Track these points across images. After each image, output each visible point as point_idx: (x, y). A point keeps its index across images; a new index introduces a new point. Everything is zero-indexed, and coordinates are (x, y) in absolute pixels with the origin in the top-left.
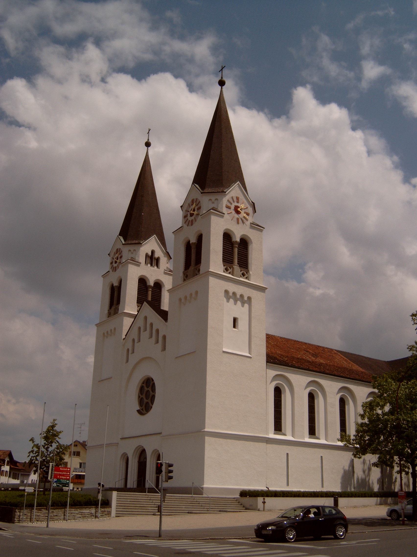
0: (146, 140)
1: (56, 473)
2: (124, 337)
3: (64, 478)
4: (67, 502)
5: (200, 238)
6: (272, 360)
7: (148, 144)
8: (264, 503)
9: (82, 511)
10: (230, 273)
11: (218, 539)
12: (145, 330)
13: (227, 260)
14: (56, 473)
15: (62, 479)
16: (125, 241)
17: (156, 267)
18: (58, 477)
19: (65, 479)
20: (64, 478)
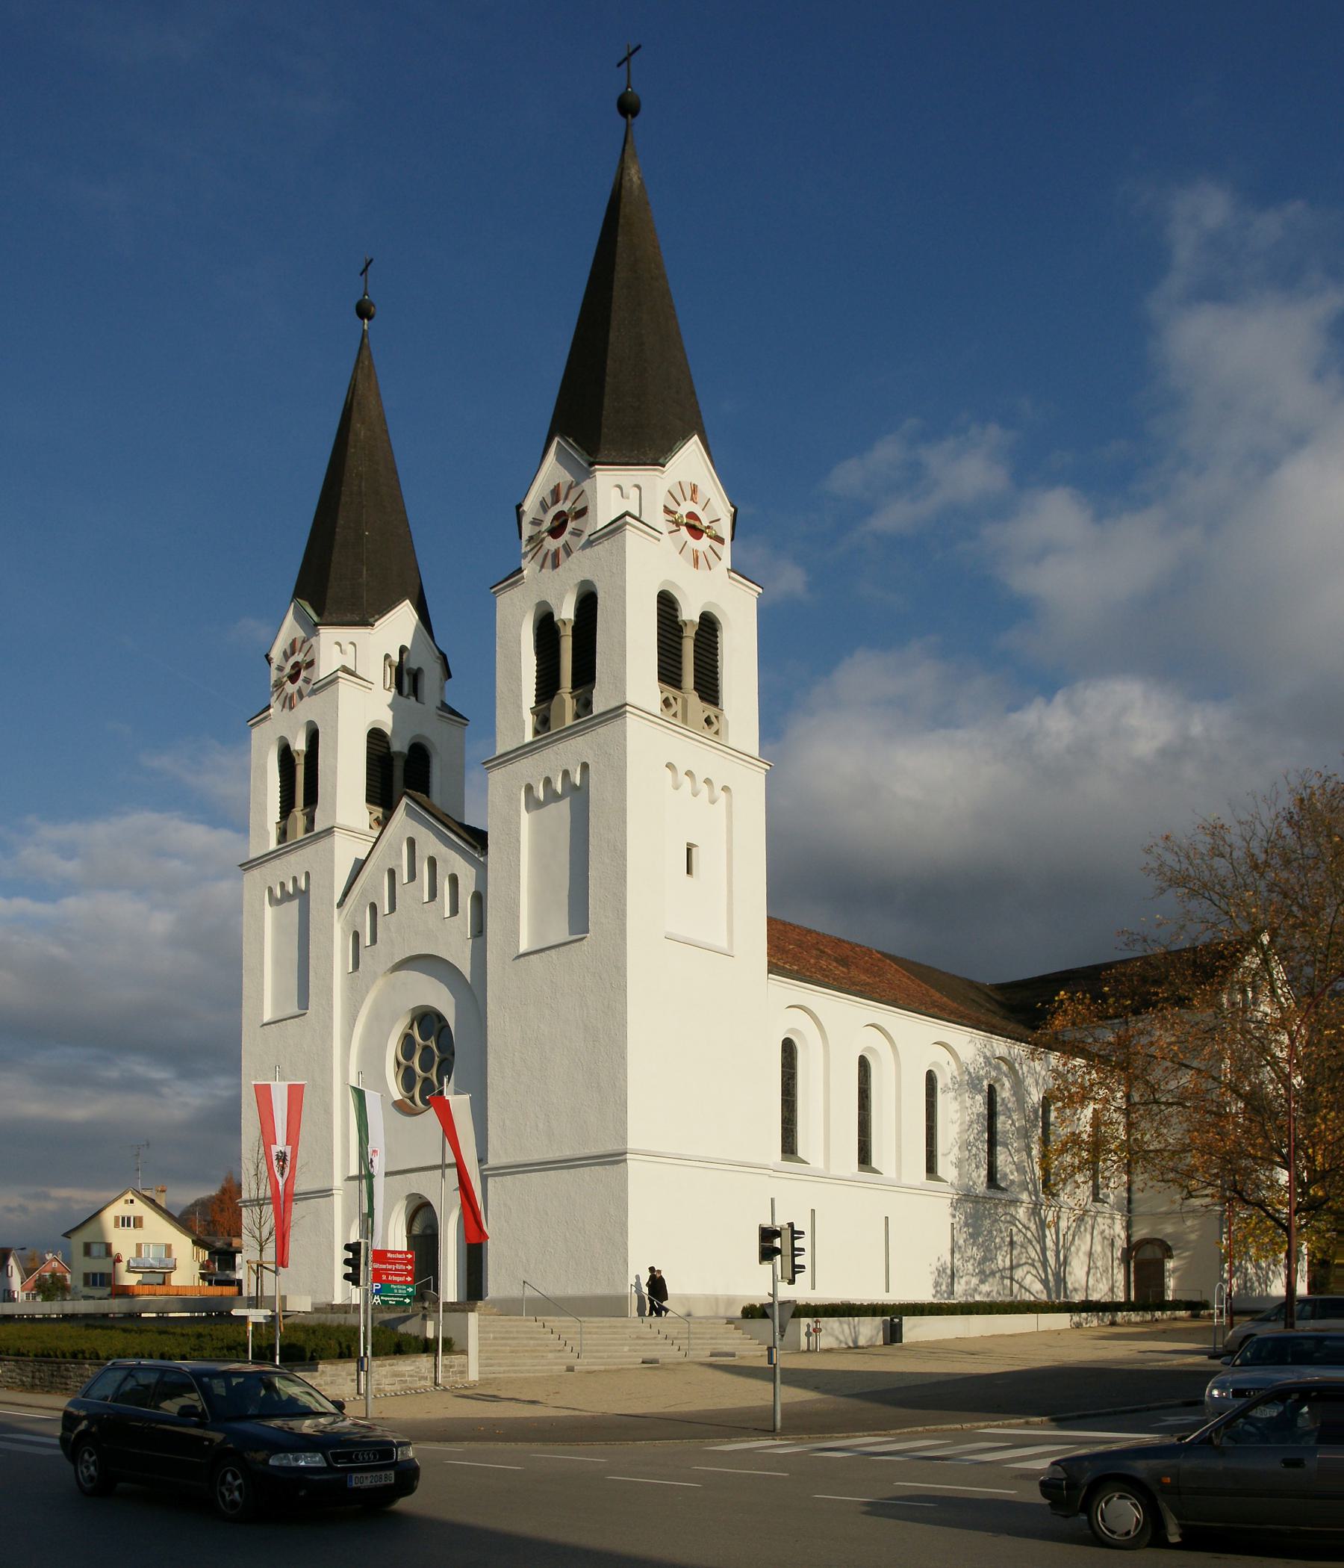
0: (621, 91)
1: (377, 1266)
2: (337, 898)
3: (398, 1279)
4: (274, 1346)
5: (587, 603)
6: (793, 952)
7: (628, 107)
8: (1112, 1289)
9: (395, 1368)
10: (675, 715)
11: (1149, 1409)
12: (412, 876)
13: (669, 673)
14: (377, 1266)
15: (395, 1283)
16: (319, 614)
17: (413, 699)
18: (384, 1277)
19: (401, 1283)
20: (398, 1279)
